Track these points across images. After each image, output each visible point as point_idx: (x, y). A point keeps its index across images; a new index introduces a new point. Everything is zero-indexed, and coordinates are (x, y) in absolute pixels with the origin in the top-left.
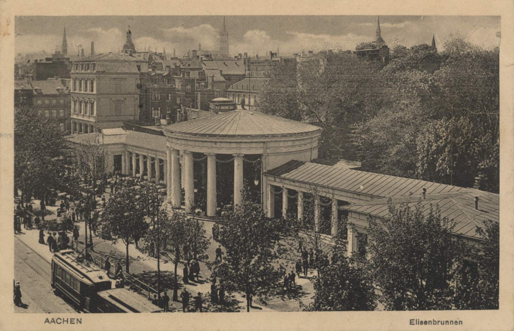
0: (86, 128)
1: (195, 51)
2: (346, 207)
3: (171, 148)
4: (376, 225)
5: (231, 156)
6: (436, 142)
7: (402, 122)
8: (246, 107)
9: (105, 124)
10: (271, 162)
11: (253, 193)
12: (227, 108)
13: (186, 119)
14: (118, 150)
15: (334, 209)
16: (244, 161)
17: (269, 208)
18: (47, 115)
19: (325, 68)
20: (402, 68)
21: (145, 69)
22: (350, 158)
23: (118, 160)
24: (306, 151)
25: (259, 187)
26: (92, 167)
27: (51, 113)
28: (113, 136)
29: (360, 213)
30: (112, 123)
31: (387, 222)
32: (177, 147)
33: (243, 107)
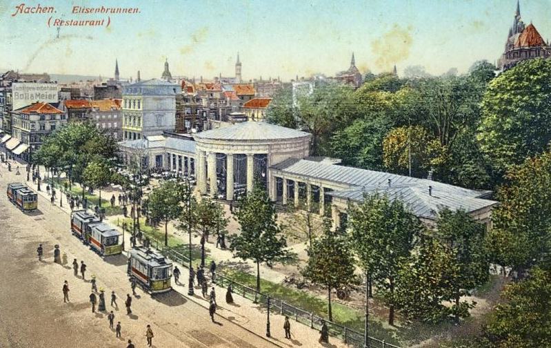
0: (135, 136)
1: (217, 78)
2: (330, 193)
3: (203, 148)
4: (353, 206)
5: (245, 155)
6: (398, 144)
7: (372, 130)
8: (256, 120)
9: (150, 133)
10: (275, 160)
11: (261, 183)
12: (241, 120)
13: (210, 129)
14: (158, 152)
15: (322, 194)
16: (234, 160)
17: (273, 194)
18: (104, 127)
19: (314, 91)
20: (372, 89)
21: (180, 92)
22: (333, 156)
23: (158, 158)
24: (300, 151)
25: (265, 178)
26: (139, 166)
27: (107, 125)
28: (157, 142)
29: (342, 198)
30: (154, 132)
31: (362, 204)
32: (205, 150)
33: (253, 119)
